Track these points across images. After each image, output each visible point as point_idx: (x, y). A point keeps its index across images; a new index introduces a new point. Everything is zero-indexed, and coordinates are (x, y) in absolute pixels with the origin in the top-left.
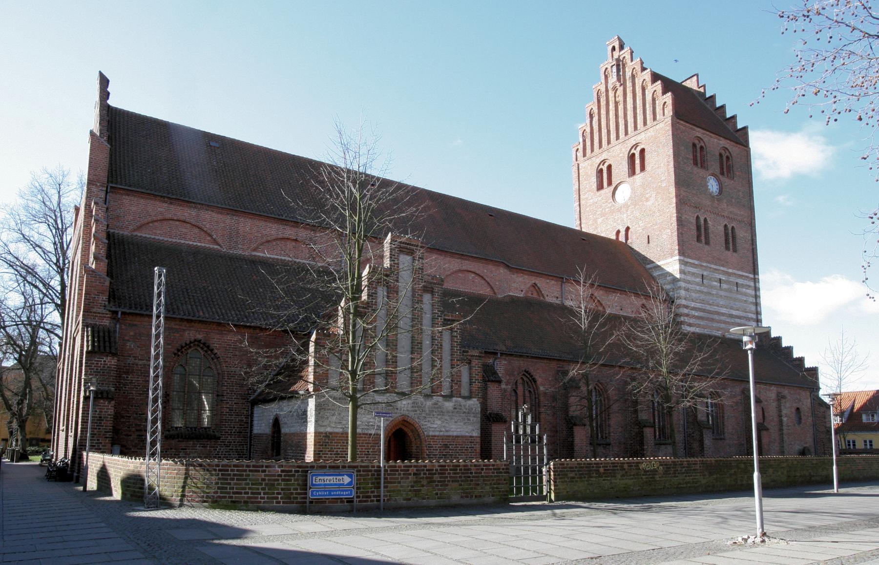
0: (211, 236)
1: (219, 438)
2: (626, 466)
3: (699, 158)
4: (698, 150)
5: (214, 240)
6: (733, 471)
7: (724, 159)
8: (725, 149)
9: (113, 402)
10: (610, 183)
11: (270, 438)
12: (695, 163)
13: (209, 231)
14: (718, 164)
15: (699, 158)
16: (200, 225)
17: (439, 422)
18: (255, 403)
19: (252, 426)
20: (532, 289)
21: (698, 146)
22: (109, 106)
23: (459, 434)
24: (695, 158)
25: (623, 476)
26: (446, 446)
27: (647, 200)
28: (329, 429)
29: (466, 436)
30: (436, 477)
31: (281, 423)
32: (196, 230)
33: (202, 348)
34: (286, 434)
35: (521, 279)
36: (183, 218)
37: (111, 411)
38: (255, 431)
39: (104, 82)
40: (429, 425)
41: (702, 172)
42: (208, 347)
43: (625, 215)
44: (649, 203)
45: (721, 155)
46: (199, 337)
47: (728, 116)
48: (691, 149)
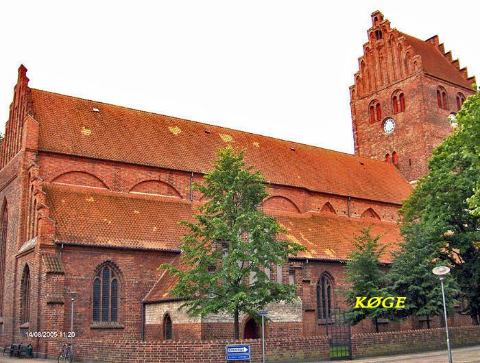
0: (102, 182)
1: (124, 328)
2: (395, 336)
3: (442, 102)
4: (442, 95)
5: (104, 184)
6: (460, 336)
7: (460, 100)
8: (460, 93)
9: (63, 306)
10: (379, 118)
11: (162, 327)
12: (440, 106)
13: (101, 178)
14: (456, 105)
15: (442, 102)
16: (95, 174)
17: (276, 313)
18: (145, 304)
19: (144, 320)
20: (326, 206)
21: (441, 92)
22: (30, 91)
23: (289, 321)
24: (439, 101)
25: (394, 342)
26: (281, 329)
27: (407, 132)
28: (209, 321)
29: (293, 322)
30: (291, 347)
31: (171, 317)
32: (92, 178)
33: (111, 266)
34: (176, 325)
35: (317, 200)
36: (84, 170)
37: (63, 312)
38: (147, 323)
39: (23, 70)
40: (270, 315)
41: (446, 112)
42: (115, 265)
43: (392, 143)
44: (409, 135)
45: (458, 98)
46: (110, 258)
47: (461, 68)
48: (436, 95)
